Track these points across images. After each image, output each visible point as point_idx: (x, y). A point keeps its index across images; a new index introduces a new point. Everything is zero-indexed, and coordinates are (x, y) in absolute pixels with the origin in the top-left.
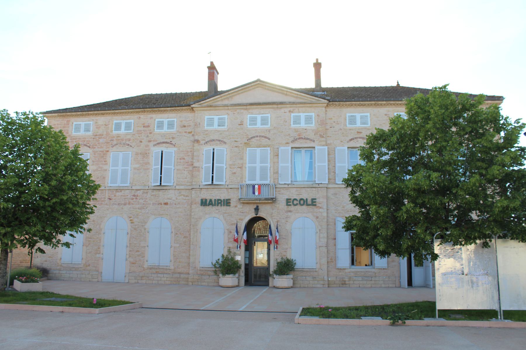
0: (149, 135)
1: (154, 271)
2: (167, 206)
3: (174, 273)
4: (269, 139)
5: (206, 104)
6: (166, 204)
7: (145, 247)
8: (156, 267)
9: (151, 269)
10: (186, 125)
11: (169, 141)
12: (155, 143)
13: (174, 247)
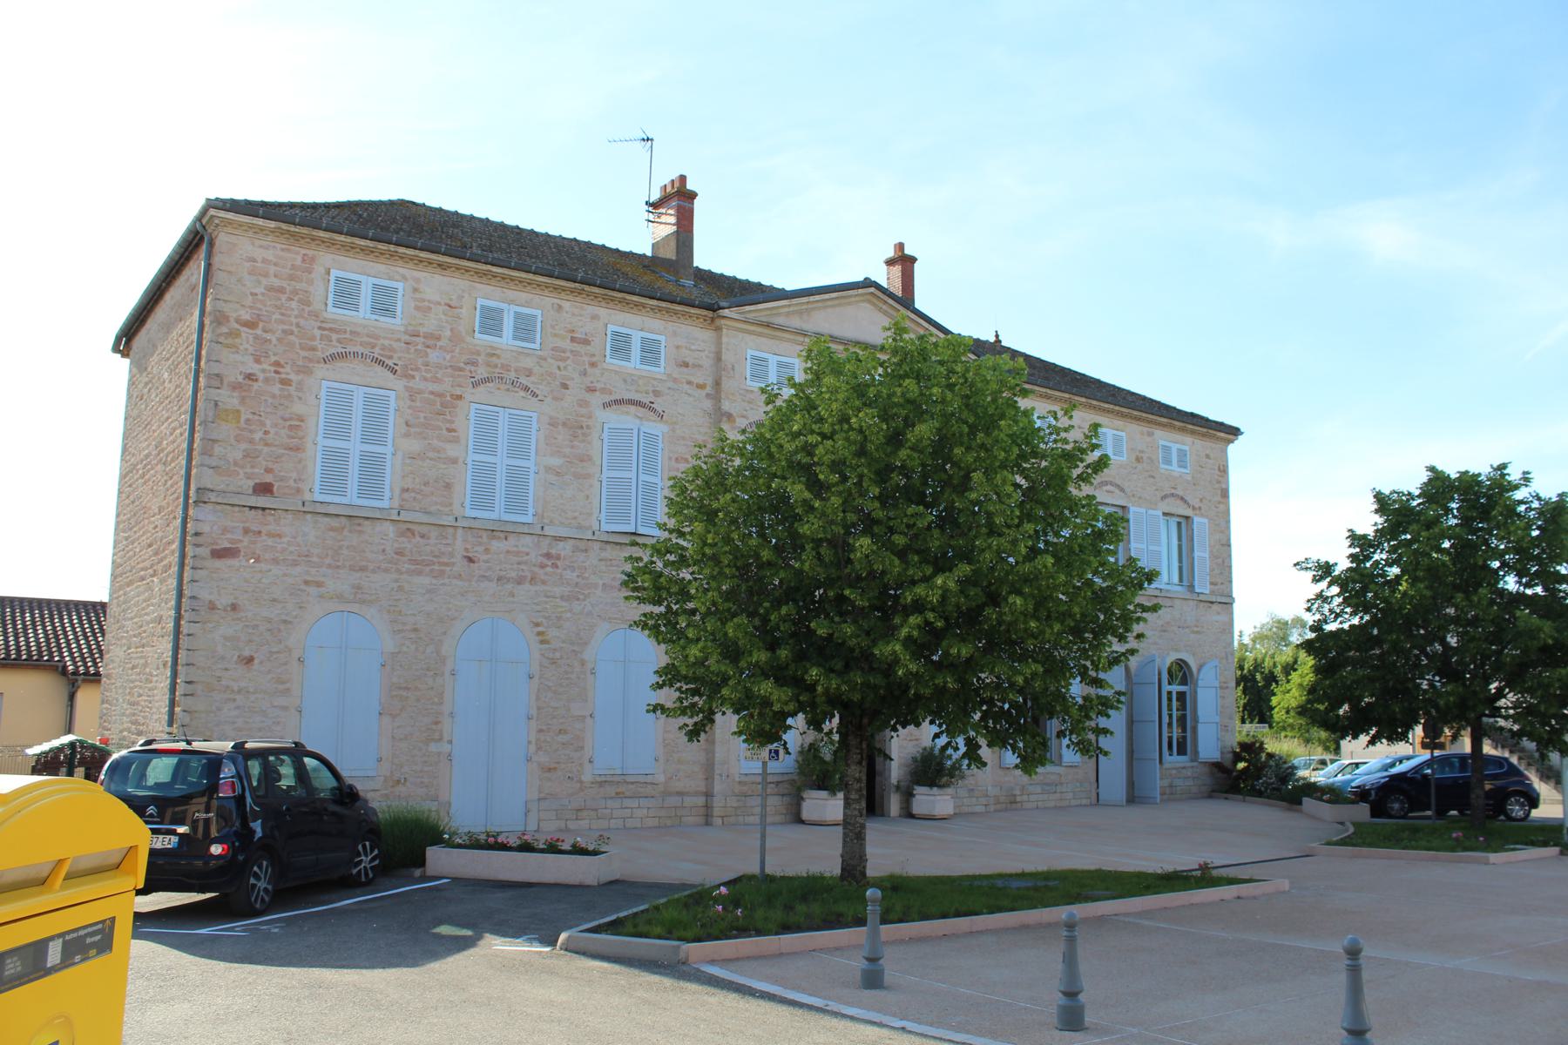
0: (590, 370)
1: (611, 791)
3: (666, 794)
7: (584, 717)
9: (601, 784)
12: (607, 398)
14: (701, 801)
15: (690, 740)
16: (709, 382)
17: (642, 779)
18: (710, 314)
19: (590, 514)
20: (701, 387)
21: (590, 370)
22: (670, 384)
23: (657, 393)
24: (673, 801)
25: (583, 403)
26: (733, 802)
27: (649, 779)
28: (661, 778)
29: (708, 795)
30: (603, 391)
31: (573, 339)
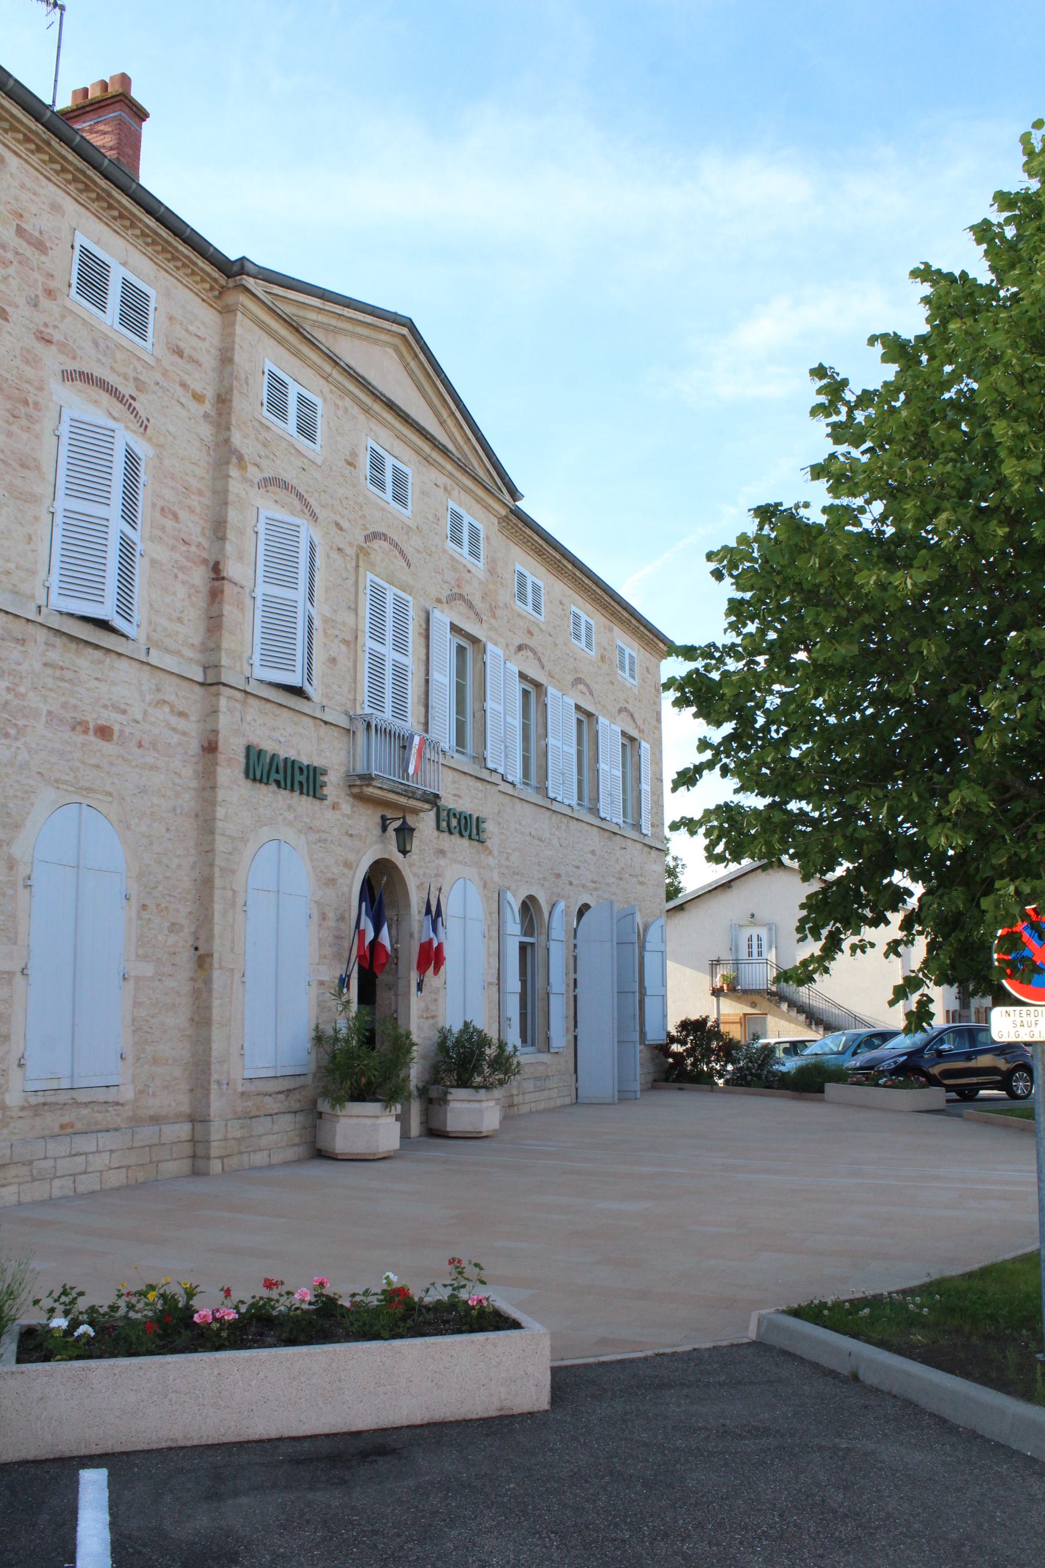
0: (45, 302)
1: (52, 1121)
2: (108, 748)
3: (137, 1121)
4: (409, 565)
5: (289, 310)
6: (104, 732)
7: (11, 974)
8: (62, 1097)
9: (37, 1110)
10: (187, 352)
11: (127, 390)
12: (71, 366)
13: (138, 979)
14: (183, 1130)
15: (713, 994)
16: (210, 393)
17: (101, 1096)
18: (222, 280)
19: (33, 573)
20: (198, 398)
21: (45, 302)
22: (158, 377)
23: (140, 385)
24: (146, 1134)
25: (31, 360)
26: (235, 1131)
27: (111, 1096)
28: (128, 1093)
29: (198, 1119)
30: (63, 347)
31: (20, 231)
